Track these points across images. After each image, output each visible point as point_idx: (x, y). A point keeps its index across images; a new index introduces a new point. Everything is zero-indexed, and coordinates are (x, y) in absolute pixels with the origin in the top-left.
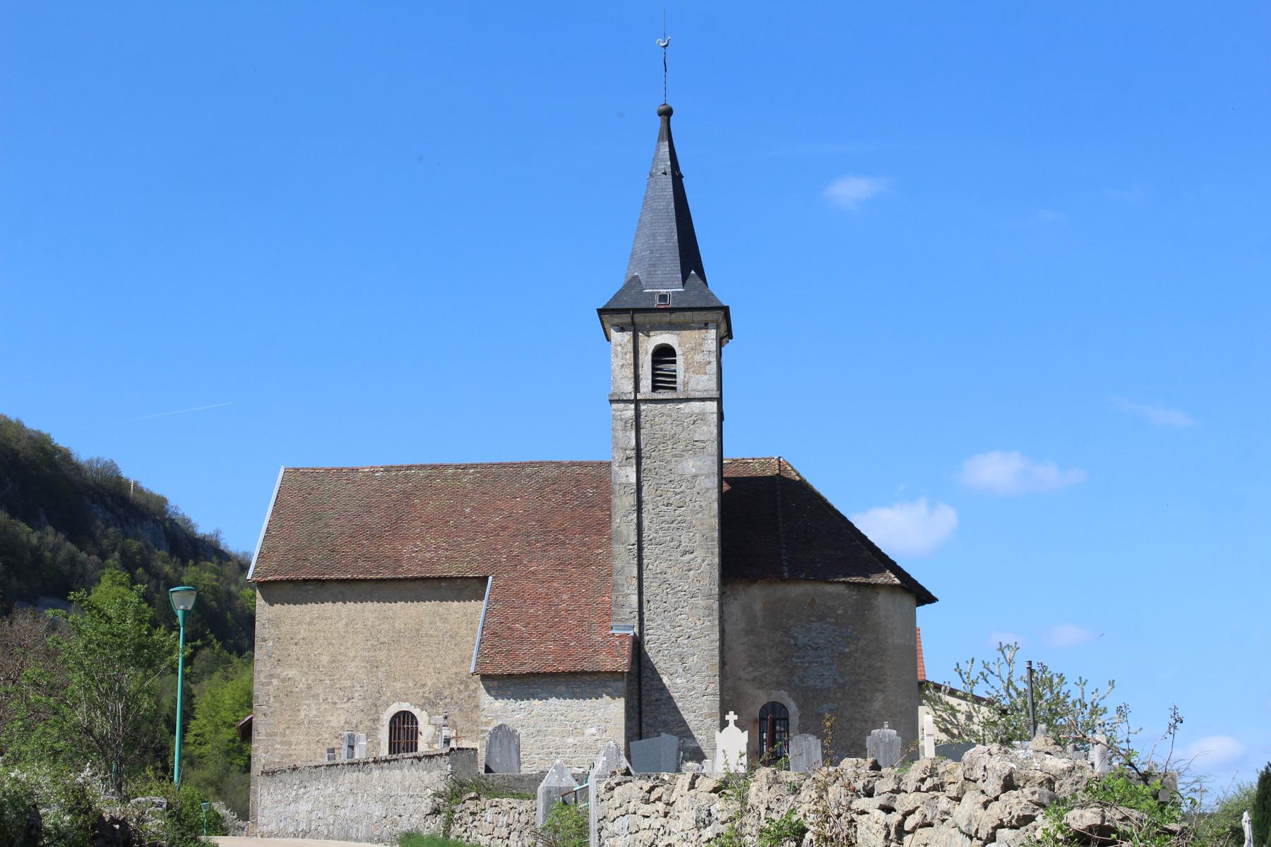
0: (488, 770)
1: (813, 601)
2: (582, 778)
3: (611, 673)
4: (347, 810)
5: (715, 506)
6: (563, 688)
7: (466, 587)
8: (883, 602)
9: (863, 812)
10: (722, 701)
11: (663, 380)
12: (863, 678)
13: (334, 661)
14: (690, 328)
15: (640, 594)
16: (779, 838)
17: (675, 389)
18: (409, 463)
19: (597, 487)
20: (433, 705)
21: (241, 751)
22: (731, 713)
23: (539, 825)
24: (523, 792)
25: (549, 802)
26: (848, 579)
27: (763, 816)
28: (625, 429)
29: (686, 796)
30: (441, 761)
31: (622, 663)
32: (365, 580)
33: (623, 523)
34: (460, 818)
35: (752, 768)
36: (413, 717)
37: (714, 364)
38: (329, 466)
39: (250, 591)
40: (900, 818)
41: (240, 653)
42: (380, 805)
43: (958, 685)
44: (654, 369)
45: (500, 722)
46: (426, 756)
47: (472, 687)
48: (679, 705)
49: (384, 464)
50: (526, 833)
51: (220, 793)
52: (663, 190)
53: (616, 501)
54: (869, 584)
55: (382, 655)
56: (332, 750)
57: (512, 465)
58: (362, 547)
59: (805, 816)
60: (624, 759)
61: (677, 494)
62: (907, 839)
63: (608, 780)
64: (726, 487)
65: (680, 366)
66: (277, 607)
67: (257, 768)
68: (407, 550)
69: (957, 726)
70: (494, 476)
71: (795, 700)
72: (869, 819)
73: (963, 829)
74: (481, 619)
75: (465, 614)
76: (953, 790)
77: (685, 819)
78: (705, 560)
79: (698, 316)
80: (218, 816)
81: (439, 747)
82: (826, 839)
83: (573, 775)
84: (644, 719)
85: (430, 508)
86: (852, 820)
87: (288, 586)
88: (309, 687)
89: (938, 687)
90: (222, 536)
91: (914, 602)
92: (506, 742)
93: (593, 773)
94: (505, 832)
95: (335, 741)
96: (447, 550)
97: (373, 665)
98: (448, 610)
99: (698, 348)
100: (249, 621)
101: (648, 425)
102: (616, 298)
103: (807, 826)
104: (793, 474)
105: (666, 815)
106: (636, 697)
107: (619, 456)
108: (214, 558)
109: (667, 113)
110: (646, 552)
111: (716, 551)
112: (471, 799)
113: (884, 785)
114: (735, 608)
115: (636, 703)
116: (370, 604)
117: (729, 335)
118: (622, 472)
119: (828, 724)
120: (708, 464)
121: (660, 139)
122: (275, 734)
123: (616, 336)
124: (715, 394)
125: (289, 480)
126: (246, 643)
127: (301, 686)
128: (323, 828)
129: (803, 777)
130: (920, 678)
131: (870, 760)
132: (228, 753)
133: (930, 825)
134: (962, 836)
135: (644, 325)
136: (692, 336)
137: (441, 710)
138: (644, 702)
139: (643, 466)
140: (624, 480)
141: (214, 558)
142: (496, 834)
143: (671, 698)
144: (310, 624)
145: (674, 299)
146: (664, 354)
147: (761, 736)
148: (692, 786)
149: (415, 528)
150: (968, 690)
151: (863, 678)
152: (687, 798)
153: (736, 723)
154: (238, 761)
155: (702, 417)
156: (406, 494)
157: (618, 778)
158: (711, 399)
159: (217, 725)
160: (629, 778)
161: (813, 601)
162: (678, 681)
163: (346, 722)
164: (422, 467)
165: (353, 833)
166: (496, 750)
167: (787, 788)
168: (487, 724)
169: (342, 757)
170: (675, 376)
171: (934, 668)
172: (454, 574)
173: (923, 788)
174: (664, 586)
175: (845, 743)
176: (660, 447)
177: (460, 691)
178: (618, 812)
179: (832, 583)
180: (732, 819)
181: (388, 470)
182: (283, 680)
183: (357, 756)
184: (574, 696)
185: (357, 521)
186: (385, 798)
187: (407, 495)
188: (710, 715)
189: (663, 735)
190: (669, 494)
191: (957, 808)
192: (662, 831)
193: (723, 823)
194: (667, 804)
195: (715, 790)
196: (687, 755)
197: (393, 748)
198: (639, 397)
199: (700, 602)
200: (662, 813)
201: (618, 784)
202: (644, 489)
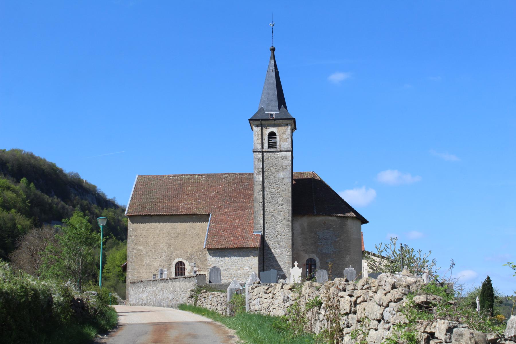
0: (210, 282)
1: (325, 222)
2: (243, 285)
5: (290, 189)
6: (236, 253)
7: (203, 218)
8: (349, 223)
9: (342, 297)
10: (293, 258)
11: (272, 144)
15: (264, 220)
16: (313, 306)
20: (191, 259)
21: (123, 275)
23: (228, 301)
28: (258, 162)
29: (280, 291)
30: (193, 279)
31: (257, 244)
32: (166, 215)
33: (258, 195)
35: (303, 281)
36: (184, 263)
39: (125, 219)
41: (122, 241)
43: (376, 252)
44: (269, 140)
47: (204, 253)
48: (277, 259)
50: (223, 304)
51: (115, 290)
55: (172, 241)
56: (155, 275)
57: (218, 174)
60: (258, 278)
62: (358, 306)
64: (294, 182)
65: (278, 139)
66: (135, 224)
68: (181, 204)
69: (376, 267)
70: (212, 178)
73: (378, 303)
76: (374, 289)
77: (280, 299)
78: (287, 208)
80: (114, 298)
81: (193, 274)
82: (329, 306)
83: (240, 284)
86: (338, 300)
88: (147, 253)
89: (369, 253)
90: (116, 199)
91: (360, 223)
93: (247, 283)
94: (216, 304)
97: (169, 245)
99: (284, 133)
100: (126, 229)
102: (255, 115)
105: (273, 298)
107: (256, 171)
109: (273, 50)
110: (266, 205)
113: (350, 287)
114: (297, 225)
116: (168, 224)
117: (295, 128)
118: (257, 177)
120: (288, 174)
122: (135, 269)
123: (255, 128)
124: (290, 149)
126: (124, 237)
130: (363, 250)
131: (345, 278)
132: (118, 276)
133: (366, 301)
134: (377, 305)
136: (283, 128)
139: (265, 175)
140: (258, 180)
142: (213, 305)
143: (274, 257)
144: (147, 230)
145: (275, 115)
148: (282, 288)
149: (184, 196)
152: (280, 292)
153: (298, 266)
155: (286, 157)
156: (180, 184)
157: (256, 285)
161: (325, 222)
162: (277, 251)
164: (187, 175)
165: (162, 304)
166: (213, 275)
168: (210, 266)
169: (158, 277)
171: (368, 246)
172: (198, 213)
173: (364, 288)
174: (272, 217)
175: (336, 272)
177: (200, 254)
178: (256, 297)
179: (332, 216)
180: (296, 299)
181: (174, 176)
182: (138, 250)
183: (164, 277)
185: (164, 194)
186: (173, 292)
187: (181, 185)
188: (288, 263)
190: (274, 185)
195: (290, 289)
197: (176, 274)
198: (263, 150)
199: (285, 223)
201: (256, 287)
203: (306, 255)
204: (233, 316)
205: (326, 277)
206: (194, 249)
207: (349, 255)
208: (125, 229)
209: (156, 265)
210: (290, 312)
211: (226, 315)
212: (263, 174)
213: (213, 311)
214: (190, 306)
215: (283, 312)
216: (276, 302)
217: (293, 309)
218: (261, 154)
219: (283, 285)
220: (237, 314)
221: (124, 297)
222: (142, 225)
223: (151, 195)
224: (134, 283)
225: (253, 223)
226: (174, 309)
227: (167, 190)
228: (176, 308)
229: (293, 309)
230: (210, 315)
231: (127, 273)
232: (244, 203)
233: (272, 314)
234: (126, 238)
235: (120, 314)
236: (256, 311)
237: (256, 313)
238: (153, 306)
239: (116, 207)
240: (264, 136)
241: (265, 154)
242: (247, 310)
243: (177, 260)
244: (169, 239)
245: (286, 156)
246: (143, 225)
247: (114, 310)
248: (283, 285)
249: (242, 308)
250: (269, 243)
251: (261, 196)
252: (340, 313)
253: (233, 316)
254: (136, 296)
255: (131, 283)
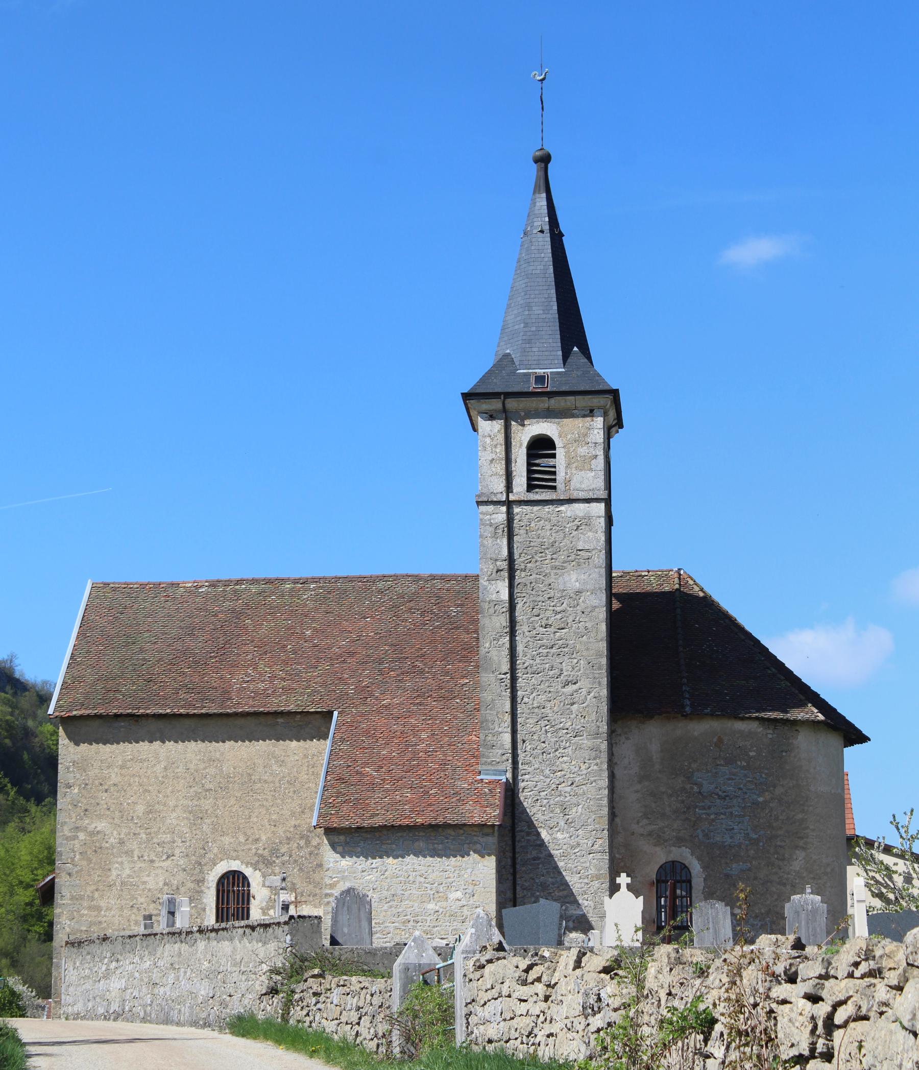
0: (334, 942)
1: (720, 740)
2: (445, 953)
3: (479, 825)
4: (168, 988)
5: (603, 627)
6: (422, 844)
7: (307, 724)
8: (803, 741)
9: (784, 1002)
10: (612, 860)
11: (540, 478)
12: (780, 832)
13: (150, 812)
14: (573, 416)
15: (514, 732)
16: (683, 1030)
17: (554, 488)
18: (239, 577)
19: (461, 605)
20: (269, 863)
21: (40, 917)
22: (623, 875)
23: (395, 1008)
24: (375, 968)
25: (407, 981)
26: (762, 715)
27: (663, 1002)
28: (495, 536)
29: (572, 979)
30: (279, 931)
31: (493, 814)
32: (187, 716)
33: (494, 650)
34: (301, 999)
35: (649, 944)
36: (245, 878)
37: (601, 459)
38: (144, 580)
39: (49, 727)
40: (829, 1009)
41: (39, 801)
42: (206, 983)
43: (894, 840)
44: (529, 464)
45: (347, 885)
46: (260, 925)
47: (315, 842)
48: (561, 864)
49: (209, 578)
50: (379, 1018)
51: (15, 965)
52: (540, 251)
53: (484, 621)
54: (787, 720)
55: (207, 804)
56: (149, 917)
57: (360, 579)
58: (178, 675)
59: (715, 1005)
60: (496, 931)
61: (557, 613)
62: (838, 1034)
63: (478, 956)
64: (616, 605)
65: (560, 461)
66: (84, 747)
67: (60, 937)
68: (236, 680)
69: (893, 890)
70: (336, 590)
71: (699, 859)
72: (792, 1010)
73: (906, 1024)
74: (325, 762)
75: (306, 756)
76: (893, 978)
77: (569, 1004)
78: (592, 692)
79: (582, 401)
80: (13, 993)
81: (275, 914)
82: (740, 1033)
83: (435, 949)
84: (519, 881)
85: (263, 631)
86: (772, 1011)
87: (97, 723)
88: (122, 842)
89: (870, 844)
90: (16, 662)
91: (842, 742)
92: (355, 907)
93: (460, 948)
94: (354, 1017)
95: (152, 906)
96: (284, 679)
97: (197, 816)
98: (285, 751)
99: (581, 439)
100: (51, 762)
101: (522, 532)
102: (483, 380)
103: (717, 1016)
104: (696, 589)
105: (547, 998)
106: (509, 854)
107: (488, 568)
108: (8, 688)
109: (544, 160)
110: (520, 683)
111: (605, 681)
112: (313, 976)
113: (810, 970)
114: (626, 749)
115: (509, 861)
116: (193, 743)
117: (619, 424)
118: (492, 588)
119: (742, 896)
120: (595, 578)
121: (536, 190)
122: (82, 898)
123: (485, 425)
124: (603, 494)
125: (97, 597)
126: (46, 788)
127: (112, 840)
128: (139, 1009)
129: (711, 956)
130: (849, 832)
131: (792, 938)
132: (24, 918)
133: (866, 1018)
134: (904, 1032)
135: (517, 412)
136: (577, 424)
137: (277, 870)
138: (518, 861)
139: (517, 581)
140: (494, 597)
141: (8, 688)
142: (343, 1019)
143: (551, 856)
144: (122, 767)
145: (551, 382)
146: (541, 447)
147: (658, 902)
148: (578, 964)
149: (247, 653)
150: (906, 847)
151: (780, 832)
152: (571, 979)
153: (629, 887)
154: (37, 928)
155: (586, 522)
156: (235, 612)
157: (489, 954)
158: (597, 500)
159: (12, 886)
160: (502, 954)
161: (720, 740)
162: (559, 835)
163: (165, 884)
164: (254, 581)
165: (174, 1015)
166: (344, 918)
167: (691, 970)
168: (332, 886)
169: (161, 926)
170: (554, 473)
171: (867, 817)
172: (292, 708)
173: (857, 974)
174: (543, 723)
175: (759, 916)
176: (537, 558)
177: (299, 847)
178: (490, 995)
179: (743, 719)
180: (626, 1006)
181: (213, 584)
182: (92, 834)
183: (178, 925)
184: (435, 853)
185: (178, 645)
186: (212, 974)
187: (237, 614)
188: (598, 877)
189: (542, 901)
190: (548, 614)
191: (898, 998)
192: (542, 1018)
193: (615, 1010)
194: (548, 986)
195: (606, 970)
196: (571, 924)
197: (221, 915)
198: (512, 497)
199: (585, 741)
200: (541, 997)
201: (490, 961)
202: (519, 607)
203: (658, 849)
204: (411, 1056)
205: (727, 930)
206: (280, 831)
207: (804, 849)
208: (50, 763)
209: (151, 885)
210: (605, 1049)
211: (389, 1056)
212: (511, 578)
213: (344, 1040)
214: (269, 1022)
215: (583, 1048)
216: (560, 1012)
217: (614, 1038)
218: (504, 509)
219: (581, 955)
220: (425, 1052)
221: (45, 990)
222: (106, 750)
223: (136, 648)
224: (80, 943)
225: (477, 743)
226: (215, 1034)
227: (191, 631)
228: (221, 1029)
229: (614, 1038)
230: (335, 1054)
231: (57, 911)
232: (447, 673)
233: (545, 1053)
234: (54, 792)
235: (32, 1049)
236: (490, 1041)
237: (490, 1048)
238: (144, 1020)
239: (18, 686)
240: (514, 450)
241: (516, 510)
242: (460, 1037)
243: (222, 868)
244: (197, 796)
245: (590, 518)
246: (108, 748)
247: (12, 1036)
248: (581, 955)
249: (445, 1032)
250: (531, 811)
251: (506, 652)
252: (775, 1057)
253: (411, 1056)
254: (87, 986)
255: (70, 944)
